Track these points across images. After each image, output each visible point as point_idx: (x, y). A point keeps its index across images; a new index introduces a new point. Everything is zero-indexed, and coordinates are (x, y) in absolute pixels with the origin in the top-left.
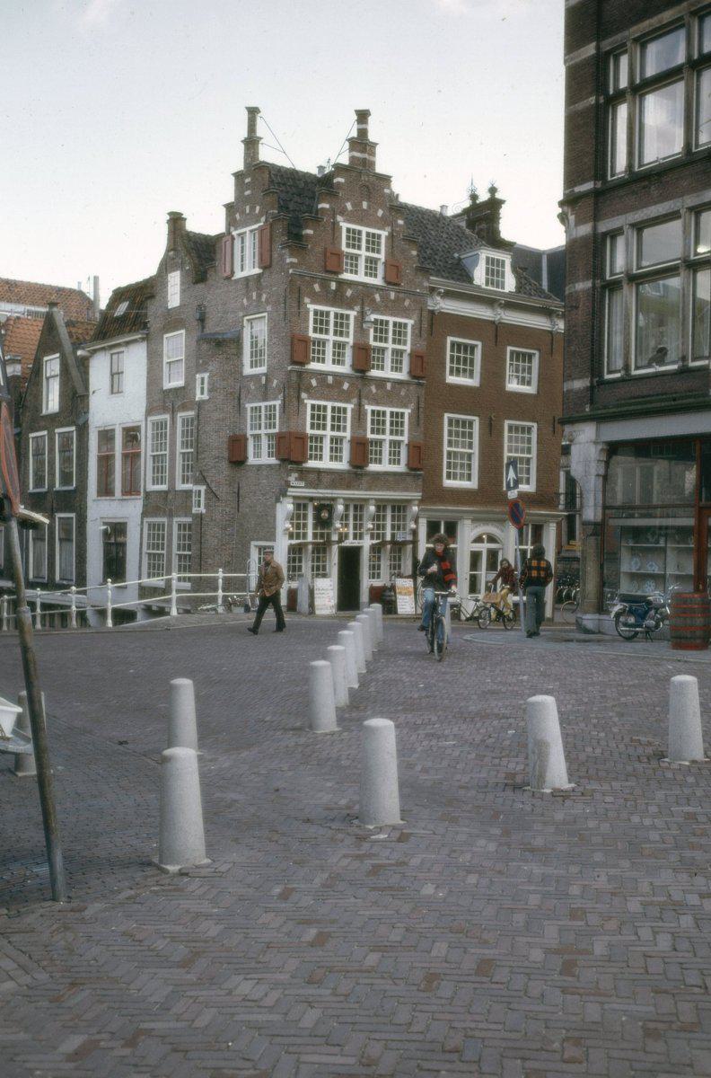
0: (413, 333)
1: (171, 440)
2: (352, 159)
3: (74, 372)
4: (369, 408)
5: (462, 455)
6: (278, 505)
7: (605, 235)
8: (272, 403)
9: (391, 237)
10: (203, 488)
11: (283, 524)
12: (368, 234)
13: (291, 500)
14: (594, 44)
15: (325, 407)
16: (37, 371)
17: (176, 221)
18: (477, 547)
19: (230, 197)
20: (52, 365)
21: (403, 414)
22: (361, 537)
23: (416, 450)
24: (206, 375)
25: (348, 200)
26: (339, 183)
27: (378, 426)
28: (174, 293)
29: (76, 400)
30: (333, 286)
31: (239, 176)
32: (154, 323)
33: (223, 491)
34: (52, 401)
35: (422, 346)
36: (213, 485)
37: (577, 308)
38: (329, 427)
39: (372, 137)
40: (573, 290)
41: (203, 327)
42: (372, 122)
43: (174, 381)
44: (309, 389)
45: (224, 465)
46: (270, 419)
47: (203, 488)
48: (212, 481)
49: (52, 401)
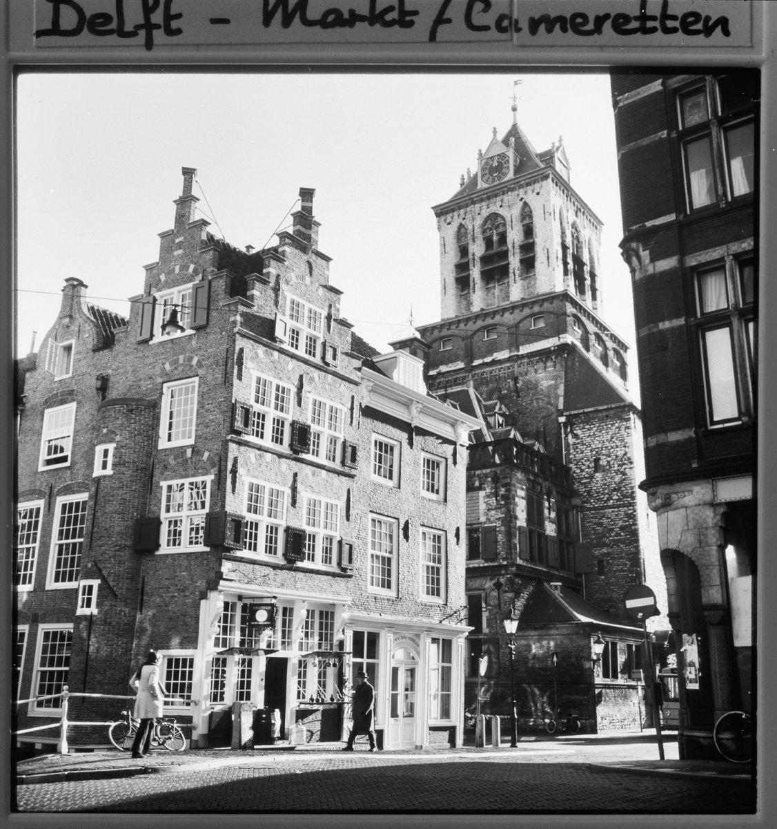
1: (44, 530)
6: (203, 602)
7: (693, 268)
8: (199, 479)
14: (660, 81)
24: (111, 447)
36: (110, 579)
37: (666, 348)
40: (655, 330)
42: (316, 199)
46: (175, 531)
48: (109, 574)
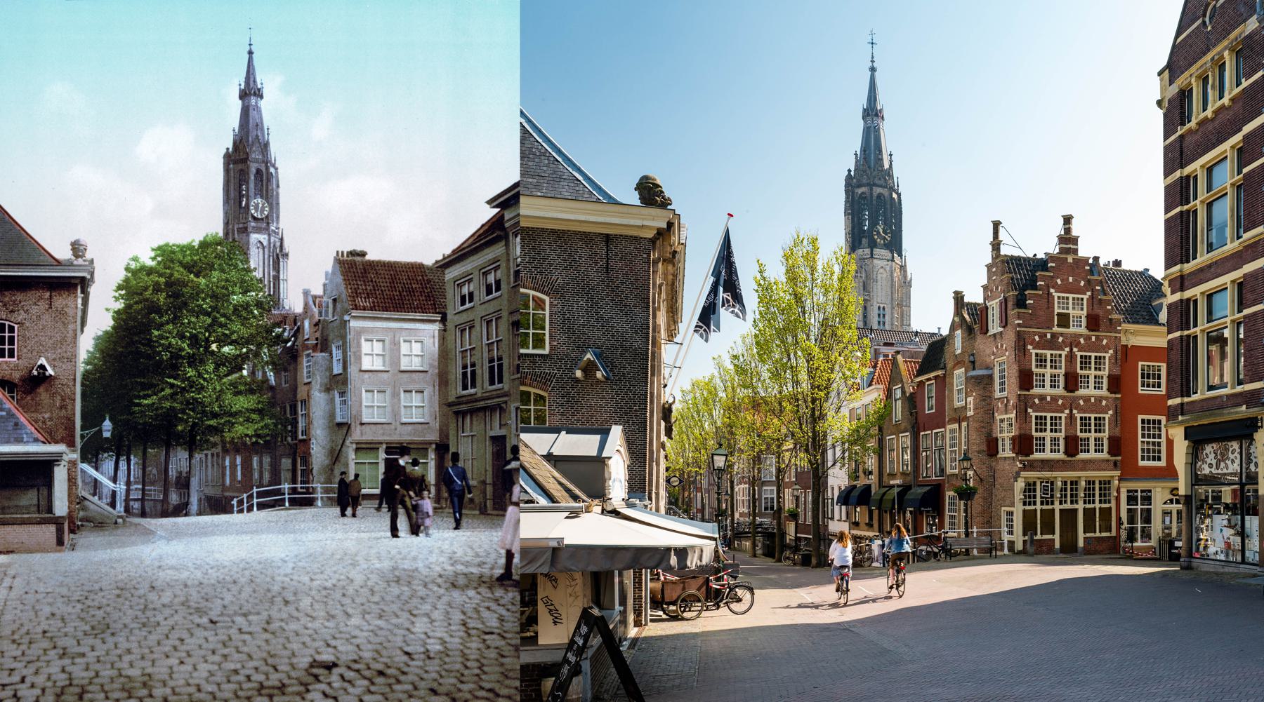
0: (1109, 362)
5: (1154, 443)
12: (1074, 299)
13: (1023, 480)
17: (959, 297)
18: (1169, 507)
22: (1077, 502)
25: (1058, 278)
26: (1051, 266)
27: (1086, 426)
28: (958, 345)
30: (1049, 336)
31: (989, 267)
39: (1074, 233)
44: (1033, 406)
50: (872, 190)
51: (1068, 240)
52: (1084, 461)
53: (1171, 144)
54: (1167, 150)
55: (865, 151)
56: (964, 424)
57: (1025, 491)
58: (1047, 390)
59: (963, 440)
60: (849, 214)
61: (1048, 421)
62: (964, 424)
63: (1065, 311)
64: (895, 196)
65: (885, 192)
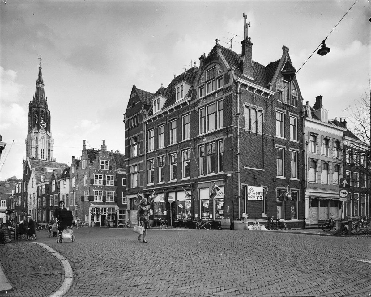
2: (102, 149)
3: (58, 185)
4: (106, 191)
9: (110, 162)
10: (77, 205)
11: (90, 211)
15: (97, 191)
16: (51, 183)
17: (73, 157)
19: (81, 155)
20: (54, 183)
21: (113, 192)
22: (106, 214)
23: (116, 199)
24: (77, 186)
28: (73, 171)
29: (58, 189)
30: (99, 170)
32: (71, 176)
33: (80, 206)
34: (54, 189)
35: (117, 180)
38: (98, 195)
39: (106, 145)
41: (78, 177)
43: (73, 186)
44: (94, 188)
45: (81, 201)
47: (77, 205)
49: (54, 189)
50: (39, 109)
51: (104, 146)
52: (107, 203)
53: (126, 131)
54: (126, 132)
55: (37, 95)
56: (75, 192)
57: (92, 210)
58: (98, 184)
59: (75, 199)
60: (30, 116)
61: (98, 192)
62: (75, 192)
63: (103, 164)
64: (48, 112)
65: (44, 110)
